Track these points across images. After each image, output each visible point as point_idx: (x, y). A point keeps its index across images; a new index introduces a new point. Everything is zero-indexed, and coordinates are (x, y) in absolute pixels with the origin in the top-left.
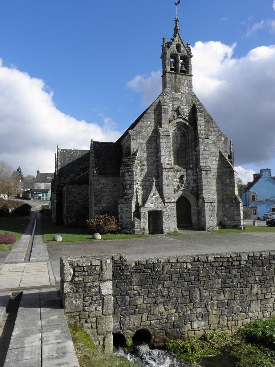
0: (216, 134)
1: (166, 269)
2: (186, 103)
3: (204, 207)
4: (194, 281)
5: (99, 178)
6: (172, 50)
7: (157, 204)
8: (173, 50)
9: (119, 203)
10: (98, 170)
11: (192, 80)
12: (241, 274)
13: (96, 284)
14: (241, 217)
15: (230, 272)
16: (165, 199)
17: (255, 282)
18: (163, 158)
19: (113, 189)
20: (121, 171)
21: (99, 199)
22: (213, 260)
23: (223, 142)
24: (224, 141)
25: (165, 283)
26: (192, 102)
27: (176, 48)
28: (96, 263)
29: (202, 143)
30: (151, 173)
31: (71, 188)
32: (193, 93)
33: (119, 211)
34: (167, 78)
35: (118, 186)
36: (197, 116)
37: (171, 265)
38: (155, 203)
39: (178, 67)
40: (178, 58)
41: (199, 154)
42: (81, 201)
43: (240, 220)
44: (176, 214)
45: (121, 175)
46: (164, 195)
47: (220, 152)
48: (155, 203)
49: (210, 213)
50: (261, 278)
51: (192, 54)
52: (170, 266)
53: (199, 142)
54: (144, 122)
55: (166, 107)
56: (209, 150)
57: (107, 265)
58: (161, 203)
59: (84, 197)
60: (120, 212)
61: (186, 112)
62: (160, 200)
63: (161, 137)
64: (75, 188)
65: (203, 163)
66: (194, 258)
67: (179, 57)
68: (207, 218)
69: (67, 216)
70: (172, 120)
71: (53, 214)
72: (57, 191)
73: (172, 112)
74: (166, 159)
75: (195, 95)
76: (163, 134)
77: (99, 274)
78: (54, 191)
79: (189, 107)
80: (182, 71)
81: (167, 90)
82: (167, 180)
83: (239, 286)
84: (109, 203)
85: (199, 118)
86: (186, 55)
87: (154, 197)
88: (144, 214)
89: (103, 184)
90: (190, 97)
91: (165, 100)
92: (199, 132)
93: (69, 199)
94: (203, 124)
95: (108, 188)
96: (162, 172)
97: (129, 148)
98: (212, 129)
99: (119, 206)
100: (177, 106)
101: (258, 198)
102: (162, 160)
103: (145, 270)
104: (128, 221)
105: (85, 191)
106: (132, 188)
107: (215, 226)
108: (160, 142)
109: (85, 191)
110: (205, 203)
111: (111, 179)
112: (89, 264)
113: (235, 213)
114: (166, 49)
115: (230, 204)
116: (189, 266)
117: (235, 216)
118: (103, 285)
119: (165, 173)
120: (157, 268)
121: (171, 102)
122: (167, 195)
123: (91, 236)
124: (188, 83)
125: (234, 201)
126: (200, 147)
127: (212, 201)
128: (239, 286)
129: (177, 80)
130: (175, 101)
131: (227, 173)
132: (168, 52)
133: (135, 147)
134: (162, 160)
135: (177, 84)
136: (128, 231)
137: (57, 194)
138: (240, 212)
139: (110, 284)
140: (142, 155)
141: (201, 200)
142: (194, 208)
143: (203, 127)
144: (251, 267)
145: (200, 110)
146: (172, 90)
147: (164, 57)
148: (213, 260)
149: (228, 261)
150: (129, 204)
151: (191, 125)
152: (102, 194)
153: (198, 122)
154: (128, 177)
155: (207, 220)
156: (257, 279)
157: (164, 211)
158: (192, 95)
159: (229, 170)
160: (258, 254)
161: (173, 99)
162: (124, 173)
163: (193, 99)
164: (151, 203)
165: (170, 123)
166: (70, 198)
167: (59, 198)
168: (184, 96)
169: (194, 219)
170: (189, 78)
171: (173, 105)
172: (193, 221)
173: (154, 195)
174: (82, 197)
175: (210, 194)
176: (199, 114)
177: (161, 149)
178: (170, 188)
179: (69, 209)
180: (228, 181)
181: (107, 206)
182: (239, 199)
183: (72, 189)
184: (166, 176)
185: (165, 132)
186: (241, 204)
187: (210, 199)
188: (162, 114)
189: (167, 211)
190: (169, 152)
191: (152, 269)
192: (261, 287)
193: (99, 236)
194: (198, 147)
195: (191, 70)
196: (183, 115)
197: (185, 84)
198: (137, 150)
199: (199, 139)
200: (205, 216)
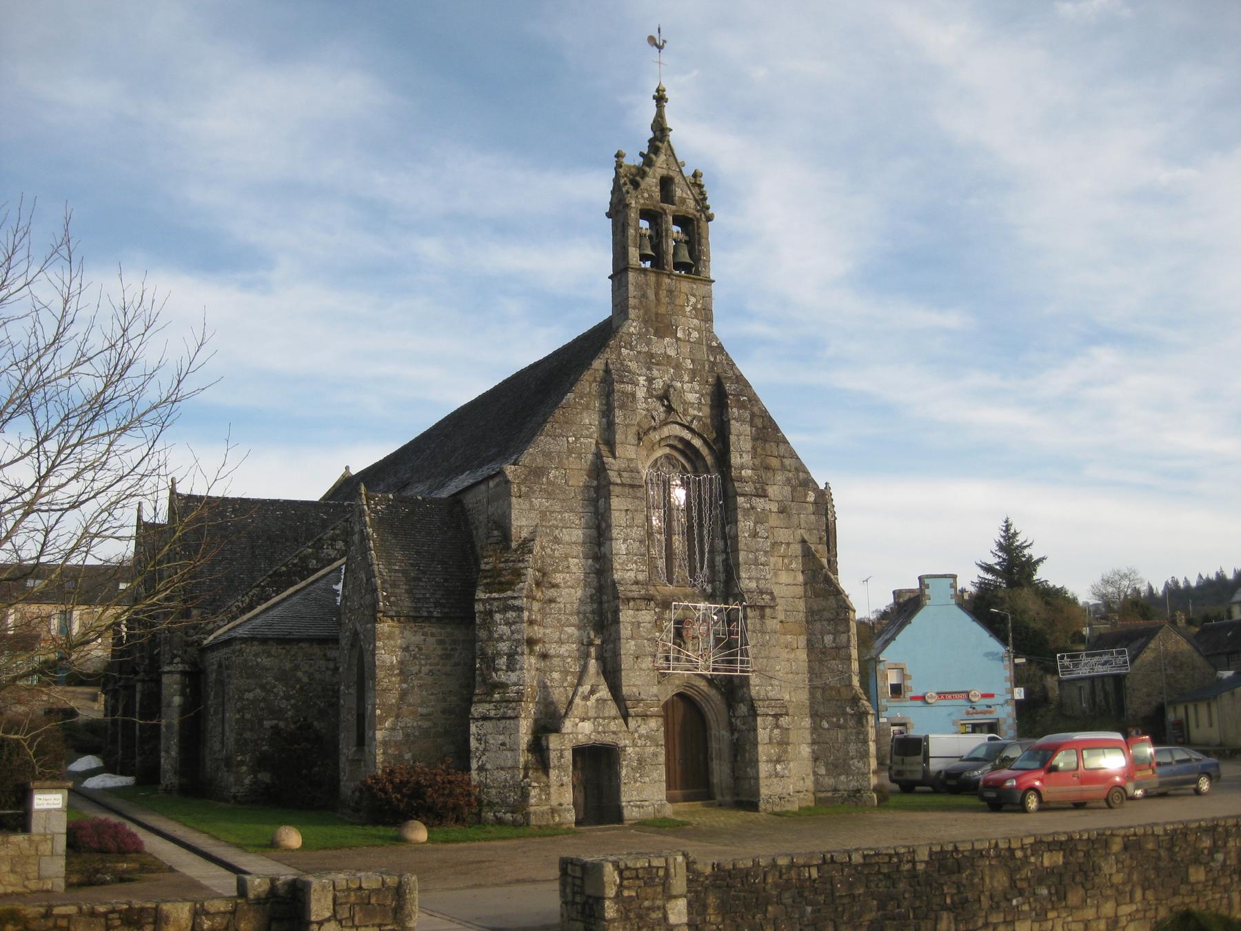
0: (788, 481)
1: (770, 880)
2: (693, 374)
3: (755, 730)
4: (824, 903)
6: (646, 195)
7: (601, 721)
8: (651, 196)
9: (474, 719)
11: (710, 297)
12: (915, 890)
13: (659, 903)
14: (871, 763)
15: (894, 886)
16: (629, 703)
17: (944, 907)
19: (439, 667)
20: (479, 607)
22: (861, 860)
23: (811, 508)
24: (815, 503)
25: (770, 908)
26: (712, 370)
27: (659, 187)
28: (656, 862)
29: (747, 512)
31: (256, 655)
33: (473, 744)
34: (630, 286)
35: (457, 655)
36: (729, 421)
37: (780, 872)
38: (595, 718)
39: (666, 253)
40: (667, 222)
41: (736, 551)
42: (292, 706)
43: (869, 773)
44: (663, 756)
45: (478, 621)
46: (625, 690)
47: (804, 541)
48: (595, 718)
49: (774, 751)
50: (956, 898)
51: (710, 211)
52: (777, 873)
53: (736, 509)
54: (555, 437)
55: (629, 388)
56: (767, 538)
57: (678, 867)
58: (615, 718)
59: (301, 688)
60: (477, 749)
61: (694, 403)
62: (612, 709)
63: (616, 490)
64: (269, 655)
65: (749, 579)
66: (824, 856)
67: (671, 219)
68: (764, 768)
69: (239, 758)
70: (649, 430)
71: (167, 752)
72: (183, 662)
74: (630, 566)
75: (720, 348)
76: (619, 481)
77: (664, 884)
78: (171, 663)
80: (678, 266)
81: (632, 329)
82: (632, 638)
83: (911, 916)
84: (427, 715)
85: (735, 426)
86: (691, 211)
87: (593, 698)
88: (562, 756)
90: (705, 353)
91: (625, 363)
92: (734, 473)
94: (748, 446)
95: (423, 662)
96: (616, 612)
97: (502, 526)
98: (775, 462)
99: (473, 728)
100: (661, 384)
101: (915, 687)
102: (617, 570)
103: (731, 881)
105: (307, 668)
106: (518, 667)
107: (789, 794)
108: (608, 508)
109: (307, 668)
110: (759, 719)
111: (434, 630)
112: (647, 865)
113: (852, 748)
114: (628, 192)
115: (835, 720)
116: (815, 873)
118: (670, 905)
119: (626, 615)
120: (752, 877)
122: (635, 690)
123: (392, 831)
124: (699, 306)
125: (848, 710)
126: (741, 524)
127: (778, 711)
128: (911, 916)
129: (663, 293)
130: (657, 364)
132: (635, 203)
133: (524, 522)
134: (617, 570)
135: (662, 310)
136: (504, 813)
137: (183, 673)
138: (868, 745)
139: (682, 904)
140: (548, 551)
141: (742, 705)
142: (719, 736)
143: (747, 458)
144: (935, 875)
145: (739, 400)
146: (647, 330)
147: (618, 211)
148: (861, 860)
149: (890, 862)
153: (733, 438)
154: (504, 629)
155: (762, 774)
156: (948, 901)
158: (710, 347)
159: (832, 602)
160: (950, 848)
161: (650, 360)
162: (490, 613)
163: (715, 358)
164: (583, 720)
165: (640, 439)
166: (249, 691)
167: (188, 690)
168: (686, 349)
169: (720, 772)
170: (700, 289)
171: (650, 380)
172: (715, 780)
173: (592, 692)
174: (294, 688)
176: (734, 412)
177: (615, 532)
178: (644, 666)
179: (248, 735)
180: (828, 639)
181: (420, 727)
182: (864, 702)
183: (259, 660)
184: (633, 623)
185: (625, 474)
186: (869, 717)
187: (773, 703)
188: (617, 410)
189: (635, 745)
190: (640, 542)
191: (744, 879)
192: (956, 919)
193: (419, 833)
194: (731, 523)
196: (684, 415)
197: (688, 309)
198: (533, 533)
199: (735, 497)
200: (757, 761)
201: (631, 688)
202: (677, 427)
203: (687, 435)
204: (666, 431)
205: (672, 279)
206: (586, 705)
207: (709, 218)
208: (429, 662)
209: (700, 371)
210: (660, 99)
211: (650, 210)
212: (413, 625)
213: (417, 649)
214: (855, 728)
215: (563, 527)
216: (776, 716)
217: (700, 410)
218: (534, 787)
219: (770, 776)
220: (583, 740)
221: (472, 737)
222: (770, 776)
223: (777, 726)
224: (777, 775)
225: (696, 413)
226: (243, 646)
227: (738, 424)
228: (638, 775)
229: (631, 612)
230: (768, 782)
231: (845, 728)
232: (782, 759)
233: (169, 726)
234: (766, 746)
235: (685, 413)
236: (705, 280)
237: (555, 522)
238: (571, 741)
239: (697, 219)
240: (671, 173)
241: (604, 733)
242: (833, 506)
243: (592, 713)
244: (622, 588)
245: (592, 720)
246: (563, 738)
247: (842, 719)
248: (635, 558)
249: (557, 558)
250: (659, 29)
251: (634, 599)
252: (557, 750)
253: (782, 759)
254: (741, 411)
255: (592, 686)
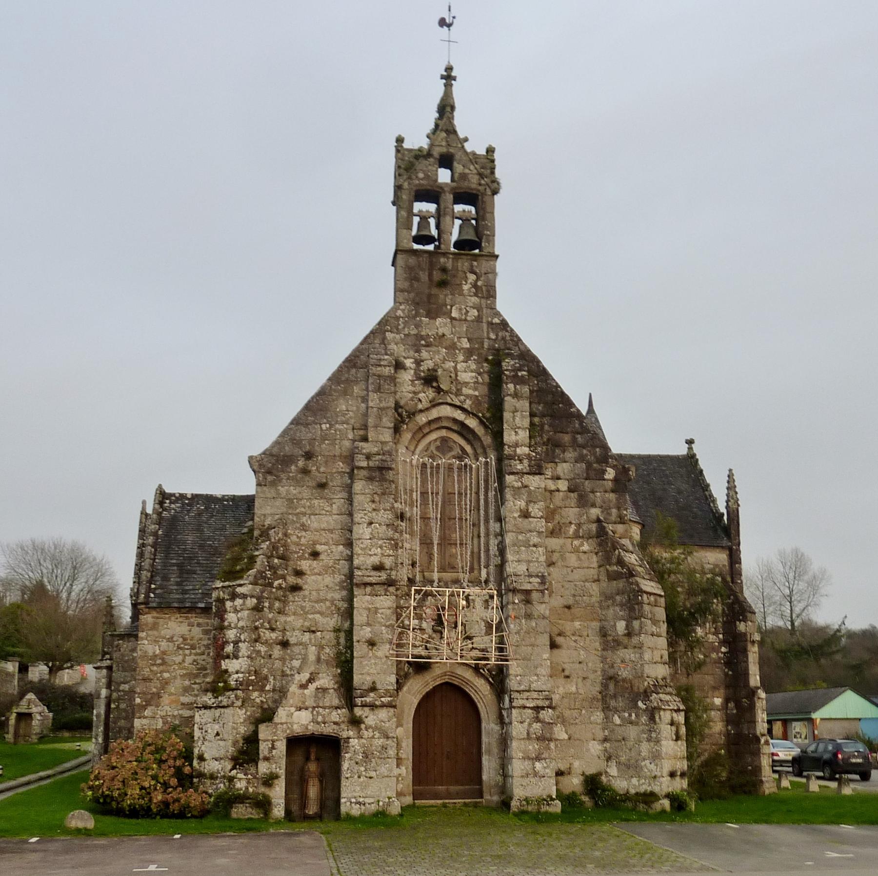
2: (469, 353)
5: (158, 618)
7: (321, 710)
10: (157, 592)
18: (362, 549)
19: (204, 657)
21: (154, 690)
24: (616, 480)
29: (517, 491)
30: (322, 601)
32: (498, 314)
38: (314, 708)
48: (314, 708)
73: (413, 385)
79: (480, 366)
82: (368, 624)
86: (474, 186)
87: (312, 687)
89: (171, 640)
93: (121, 688)
95: (187, 652)
104: (218, 770)
111: (201, 620)
115: (626, 715)
117: (644, 759)
121: (412, 353)
127: (540, 703)
131: (618, 598)
133: (268, 510)
143: (523, 435)
145: (516, 376)
150: (222, 710)
151: (486, 427)
152: (166, 675)
153: (507, 415)
157: (349, 738)
163: (497, 335)
171: (418, 362)
173: (311, 680)
175: (537, 675)
181: (181, 716)
184: (369, 609)
189: (360, 737)
195: (494, 236)
201: (364, 676)
202: (448, 407)
203: (459, 415)
204: (434, 413)
205: (448, 258)
206: (304, 693)
207: (495, 192)
208: (193, 651)
209: (478, 349)
210: (448, 77)
211: (429, 190)
212: (179, 615)
213: (181, 640)
214: (647, 725)
215: (310, 515)
216: (537, 709)
217: (475, 389)
218: (240, 779)
219: (527, 775)
220: (299, 731)
221: (196, 726)
222: (527, 775)
223: (537, 720)
224: (536, 774)
225: (471, 392)
226: (120, 642)
227: (514, 401)
228: (363, 769)
229: (368, 598)
230: (525, 781)
231: (637, 724)
232: (543, 756)
233: (98, 716)
234: (522, 742)
235: (458, 393)
236: (487, 256)
237: (303, 510)
238: (284, 731)
239: (482, 194)
240: (452, 150)
241: (324, 723)
242: (736, 493)
243: (310, 702)
244: (360, 573)
245: (310, 709)
246: (276, 728)
247: (633, 715)
248: (380, 542)
249: (302, 545)
250: (450, 7)
251: (371, 584)
252: (268, 740)
253: (543, 756)
254: (518, 387)
255: (311, 674)
